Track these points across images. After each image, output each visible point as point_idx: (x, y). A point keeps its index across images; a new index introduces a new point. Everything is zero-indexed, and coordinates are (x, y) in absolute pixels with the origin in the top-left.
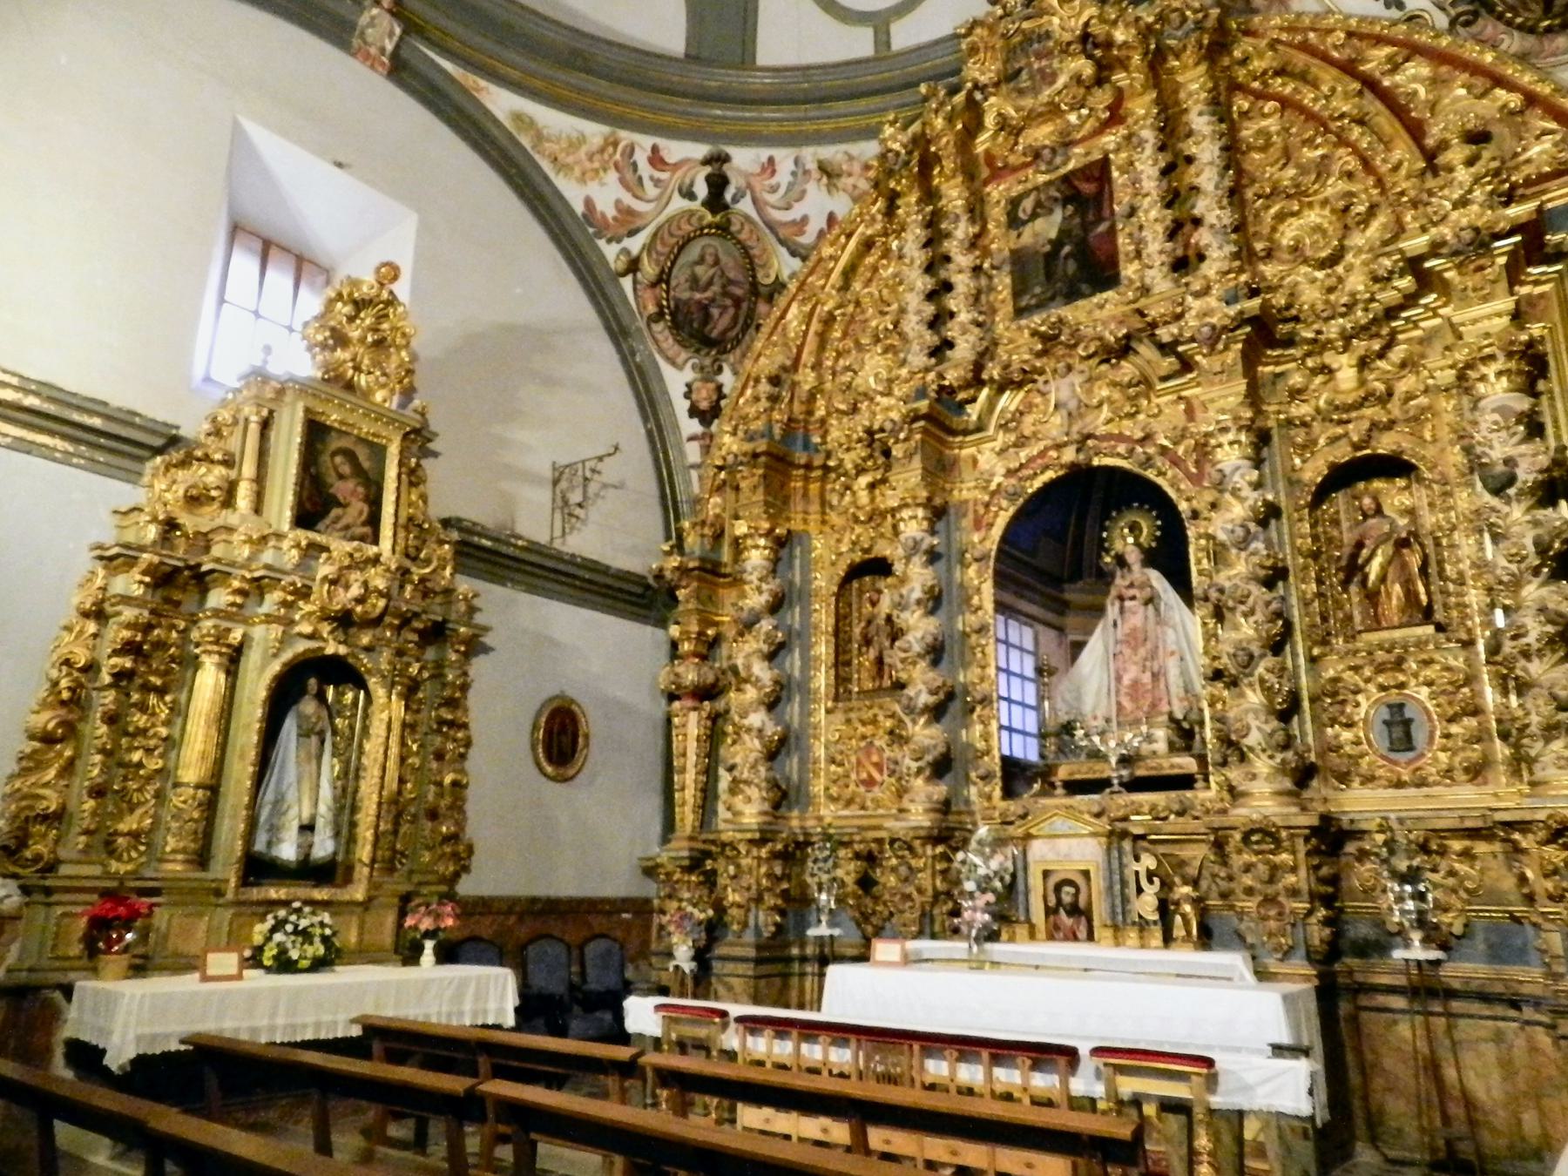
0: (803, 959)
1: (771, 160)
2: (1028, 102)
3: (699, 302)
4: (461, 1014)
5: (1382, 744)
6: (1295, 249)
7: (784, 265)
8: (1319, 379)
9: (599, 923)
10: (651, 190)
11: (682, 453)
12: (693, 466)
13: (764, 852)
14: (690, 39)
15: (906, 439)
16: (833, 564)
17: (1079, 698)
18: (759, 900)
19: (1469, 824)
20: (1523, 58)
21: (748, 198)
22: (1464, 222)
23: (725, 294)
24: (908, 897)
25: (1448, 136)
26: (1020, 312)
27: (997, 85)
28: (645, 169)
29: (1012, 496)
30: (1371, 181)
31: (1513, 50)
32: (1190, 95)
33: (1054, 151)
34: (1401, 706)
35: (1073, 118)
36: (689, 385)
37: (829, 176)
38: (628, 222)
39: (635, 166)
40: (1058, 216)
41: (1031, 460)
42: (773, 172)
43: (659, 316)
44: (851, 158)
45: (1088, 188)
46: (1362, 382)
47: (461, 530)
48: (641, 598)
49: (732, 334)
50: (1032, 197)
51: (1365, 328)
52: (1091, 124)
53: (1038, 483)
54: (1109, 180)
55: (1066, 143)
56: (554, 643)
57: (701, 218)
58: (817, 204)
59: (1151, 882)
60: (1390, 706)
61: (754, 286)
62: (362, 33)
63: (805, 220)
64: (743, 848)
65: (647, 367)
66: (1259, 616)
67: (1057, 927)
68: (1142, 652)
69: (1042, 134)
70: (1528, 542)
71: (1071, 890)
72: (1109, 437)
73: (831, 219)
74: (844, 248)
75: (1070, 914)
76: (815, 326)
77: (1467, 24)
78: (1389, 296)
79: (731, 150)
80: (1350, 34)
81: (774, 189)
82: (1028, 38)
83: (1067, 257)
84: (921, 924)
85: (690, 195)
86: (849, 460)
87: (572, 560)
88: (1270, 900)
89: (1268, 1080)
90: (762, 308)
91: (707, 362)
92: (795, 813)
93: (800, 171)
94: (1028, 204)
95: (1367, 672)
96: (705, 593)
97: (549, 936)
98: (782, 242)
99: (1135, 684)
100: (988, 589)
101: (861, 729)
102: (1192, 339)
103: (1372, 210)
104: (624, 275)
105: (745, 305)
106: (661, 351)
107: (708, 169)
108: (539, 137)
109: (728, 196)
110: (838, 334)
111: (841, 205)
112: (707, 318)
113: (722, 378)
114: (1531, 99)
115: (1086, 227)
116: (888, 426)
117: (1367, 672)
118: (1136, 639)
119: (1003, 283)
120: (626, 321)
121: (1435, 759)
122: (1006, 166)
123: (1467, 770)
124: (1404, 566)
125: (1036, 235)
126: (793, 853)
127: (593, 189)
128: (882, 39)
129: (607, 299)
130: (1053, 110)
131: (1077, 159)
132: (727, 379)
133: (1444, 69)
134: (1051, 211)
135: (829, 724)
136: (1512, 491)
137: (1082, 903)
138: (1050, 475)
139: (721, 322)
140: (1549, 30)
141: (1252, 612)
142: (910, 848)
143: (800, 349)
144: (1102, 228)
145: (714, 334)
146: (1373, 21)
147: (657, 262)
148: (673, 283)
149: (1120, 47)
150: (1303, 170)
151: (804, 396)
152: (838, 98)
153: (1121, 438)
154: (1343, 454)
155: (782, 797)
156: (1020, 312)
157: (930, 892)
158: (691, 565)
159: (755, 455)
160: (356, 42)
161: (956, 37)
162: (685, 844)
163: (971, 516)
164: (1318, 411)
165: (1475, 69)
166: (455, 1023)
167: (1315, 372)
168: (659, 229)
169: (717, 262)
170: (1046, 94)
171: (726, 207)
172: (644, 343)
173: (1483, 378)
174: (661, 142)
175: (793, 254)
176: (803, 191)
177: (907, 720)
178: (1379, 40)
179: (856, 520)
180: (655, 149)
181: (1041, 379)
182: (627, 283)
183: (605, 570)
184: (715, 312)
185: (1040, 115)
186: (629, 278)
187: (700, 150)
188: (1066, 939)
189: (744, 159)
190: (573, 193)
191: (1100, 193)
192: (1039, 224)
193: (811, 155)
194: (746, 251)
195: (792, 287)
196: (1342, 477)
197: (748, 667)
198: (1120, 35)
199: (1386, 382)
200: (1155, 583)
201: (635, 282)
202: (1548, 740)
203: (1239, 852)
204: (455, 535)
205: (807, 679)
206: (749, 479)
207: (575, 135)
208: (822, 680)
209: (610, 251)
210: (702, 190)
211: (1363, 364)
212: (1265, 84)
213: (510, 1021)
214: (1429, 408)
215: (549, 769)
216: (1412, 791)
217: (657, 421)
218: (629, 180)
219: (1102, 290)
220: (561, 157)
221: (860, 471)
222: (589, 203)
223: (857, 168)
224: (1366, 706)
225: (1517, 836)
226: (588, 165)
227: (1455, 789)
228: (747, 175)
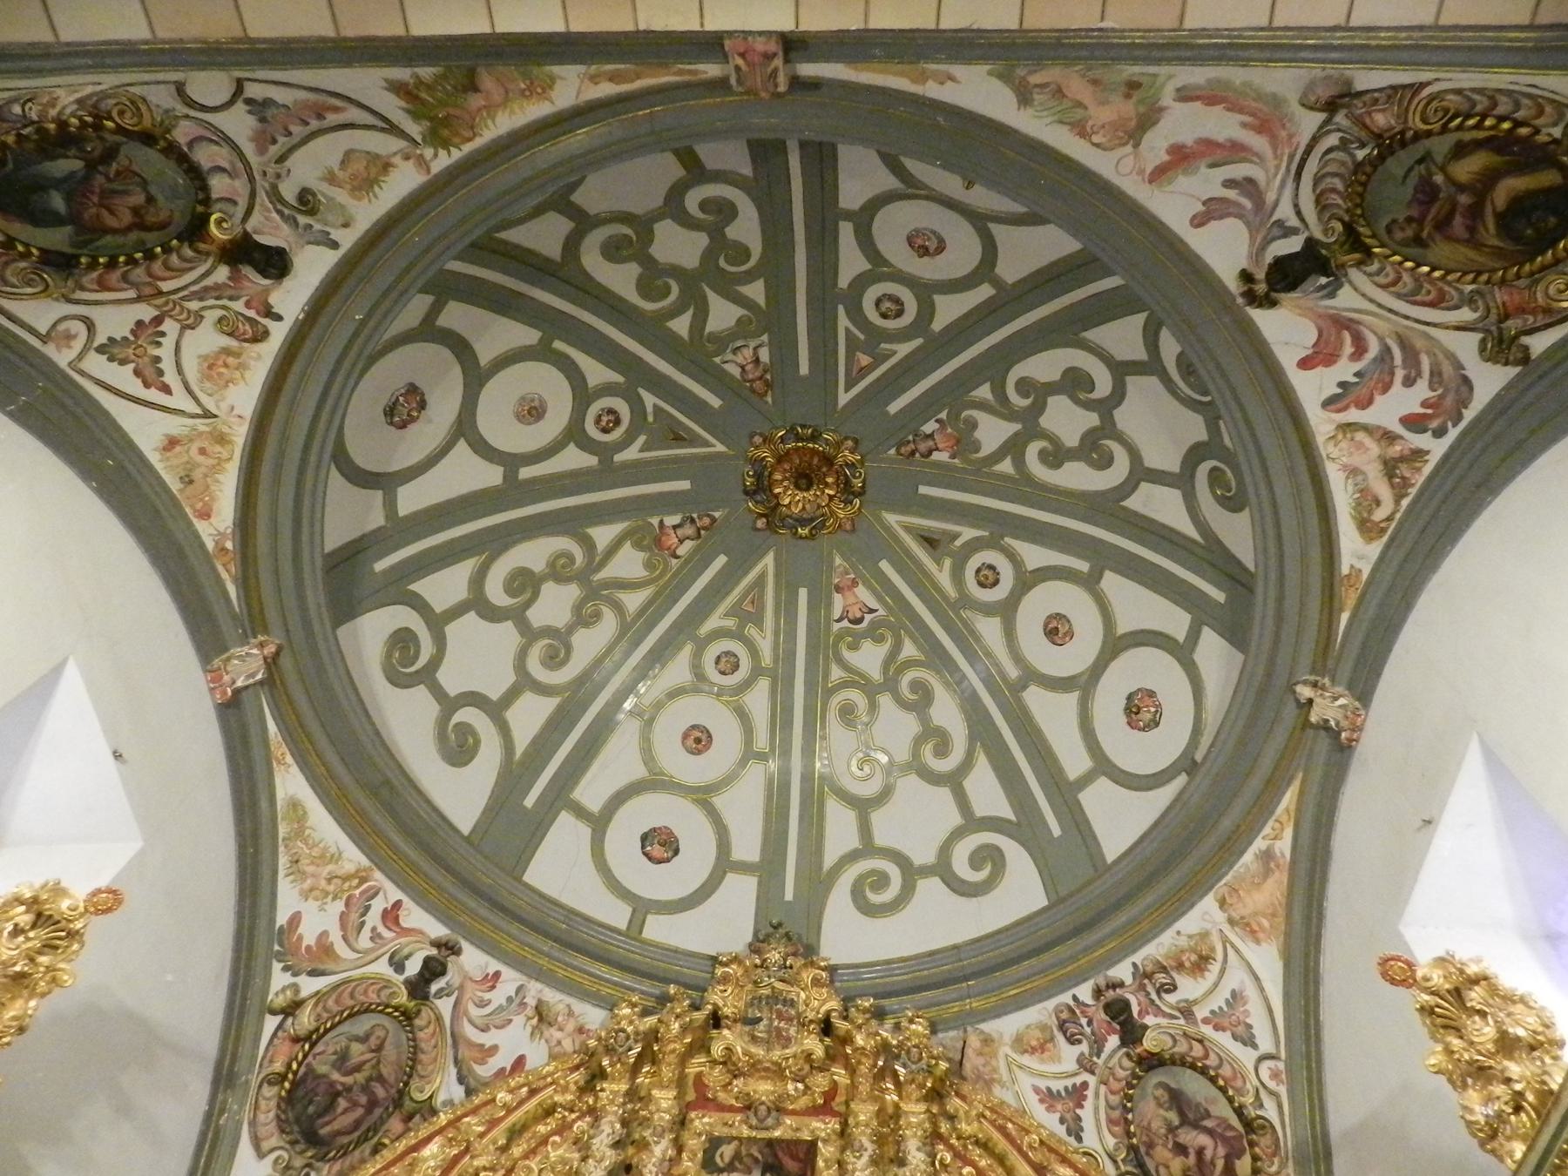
1: (497, 975)
2: (759, 1052)
3: (332, 1084)
7: (446, 1087)
10: (364, 941)
14: (472, 832)
21: (453, 999)
28: (373, 918)
32: (909, 1124)
35: (790, 1087)
37: (541, 1019)
38: (320, 958)
42: (493, 987)
44: (570, 1013)
49: (345, 1140)
50: (735, 1144)
52: (804, 1102)
55: (779, 1109)
58: (514, 1040)
62: (228, 659)
63: (494, 1050)
69: (763, 1089)
73: (520, 1062)
74: (521, 1103)
79: (465, 945)
82: (775, 998)
85: (399, 967)
90: (395, 1124)
91: (298, 1162)
94: (727, 1151)
98: (456, 1062)
104: (274, 1013)
105: (378, 1112)
106: (253, 1123)
107: (434, 952)
108: (299, 833)
109: (434, 988)
111: (537, 1056)
112: (330, 1107)
120: (241, 1065)
127: (309, 909)
128: (637, 923)
129: (239, 1028)
130: (777, 1072)
148: (319, 1048)
149: (855, 1050)
160: (217, 662)
161: (714, 960)
169: (379, 1049)
170: (776, 1054)
171: (426, 997)
172: (242, 1106)
174: (408, 903)
176: (508, 1023)
180: (398, 905)
182: (271, 1023)
184: (342, 1103)
185: (766, 1069)
187: (438, 930)
189: (472, 960)
190: (287, 899)
193: (536, 990)
194: (416, 1049)
195: (443, 1119)
198: (860, 1040)
201: (280, 1026)
207: (333, 850)
209: (279, 979)
210: (413, 967)
218: (345, 916)
220: (304, 861)
222: (295, 919)
223: (570, 1026)
226: (323, 883)
228: (467, 977)
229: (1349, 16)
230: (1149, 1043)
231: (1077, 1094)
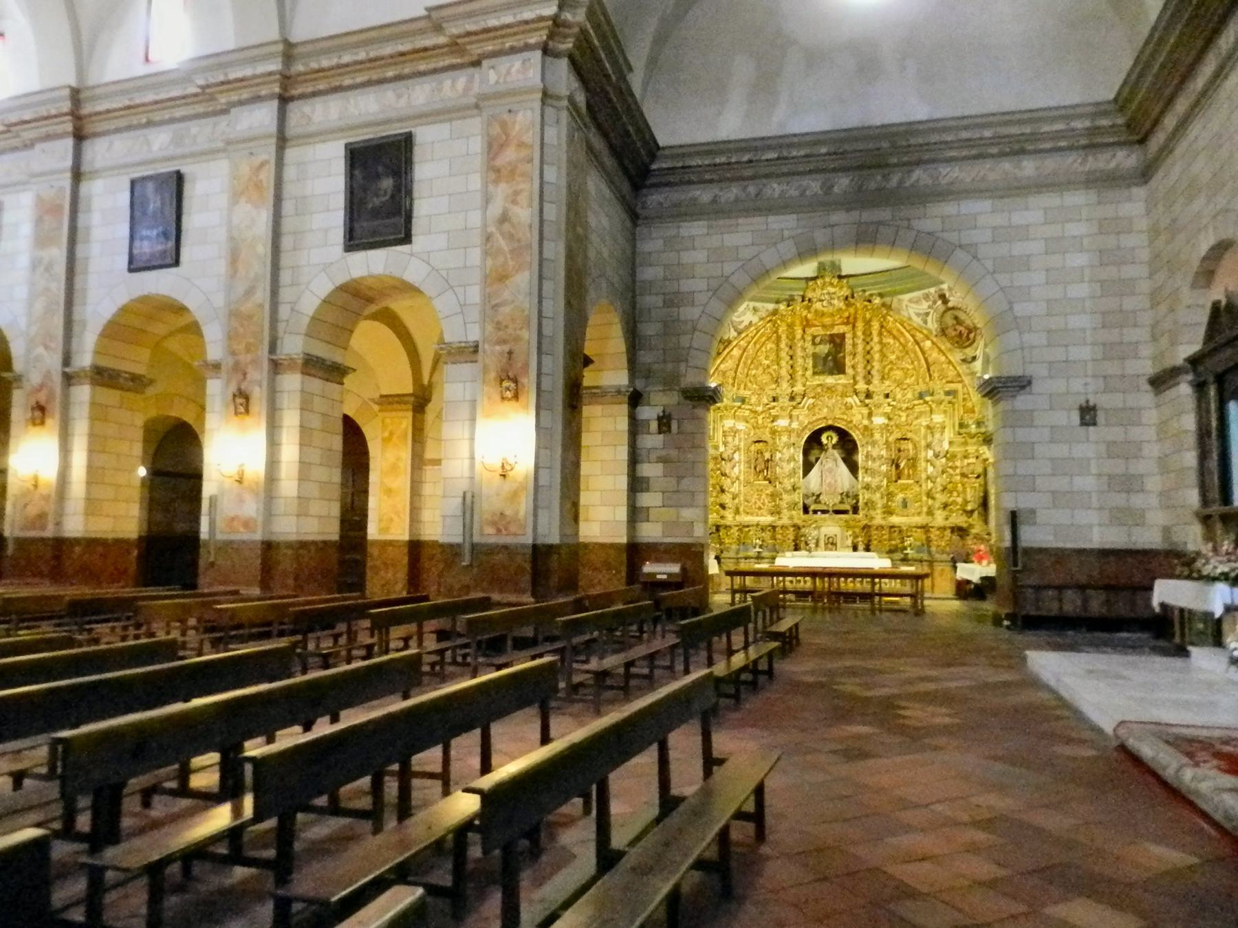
26: (815, 373)
45: (838, 341)
55: (833, 326)
69: (827, 320)
75: (831, 544)
94: (818, 340)
111: (755, 319)
118: (830, 471)
119: (810, 362)
131: (836, 330)
156: (815, 373)
192: (821, 347)
229: (415, 511)
230: (950, 305)
231: (927, 314)
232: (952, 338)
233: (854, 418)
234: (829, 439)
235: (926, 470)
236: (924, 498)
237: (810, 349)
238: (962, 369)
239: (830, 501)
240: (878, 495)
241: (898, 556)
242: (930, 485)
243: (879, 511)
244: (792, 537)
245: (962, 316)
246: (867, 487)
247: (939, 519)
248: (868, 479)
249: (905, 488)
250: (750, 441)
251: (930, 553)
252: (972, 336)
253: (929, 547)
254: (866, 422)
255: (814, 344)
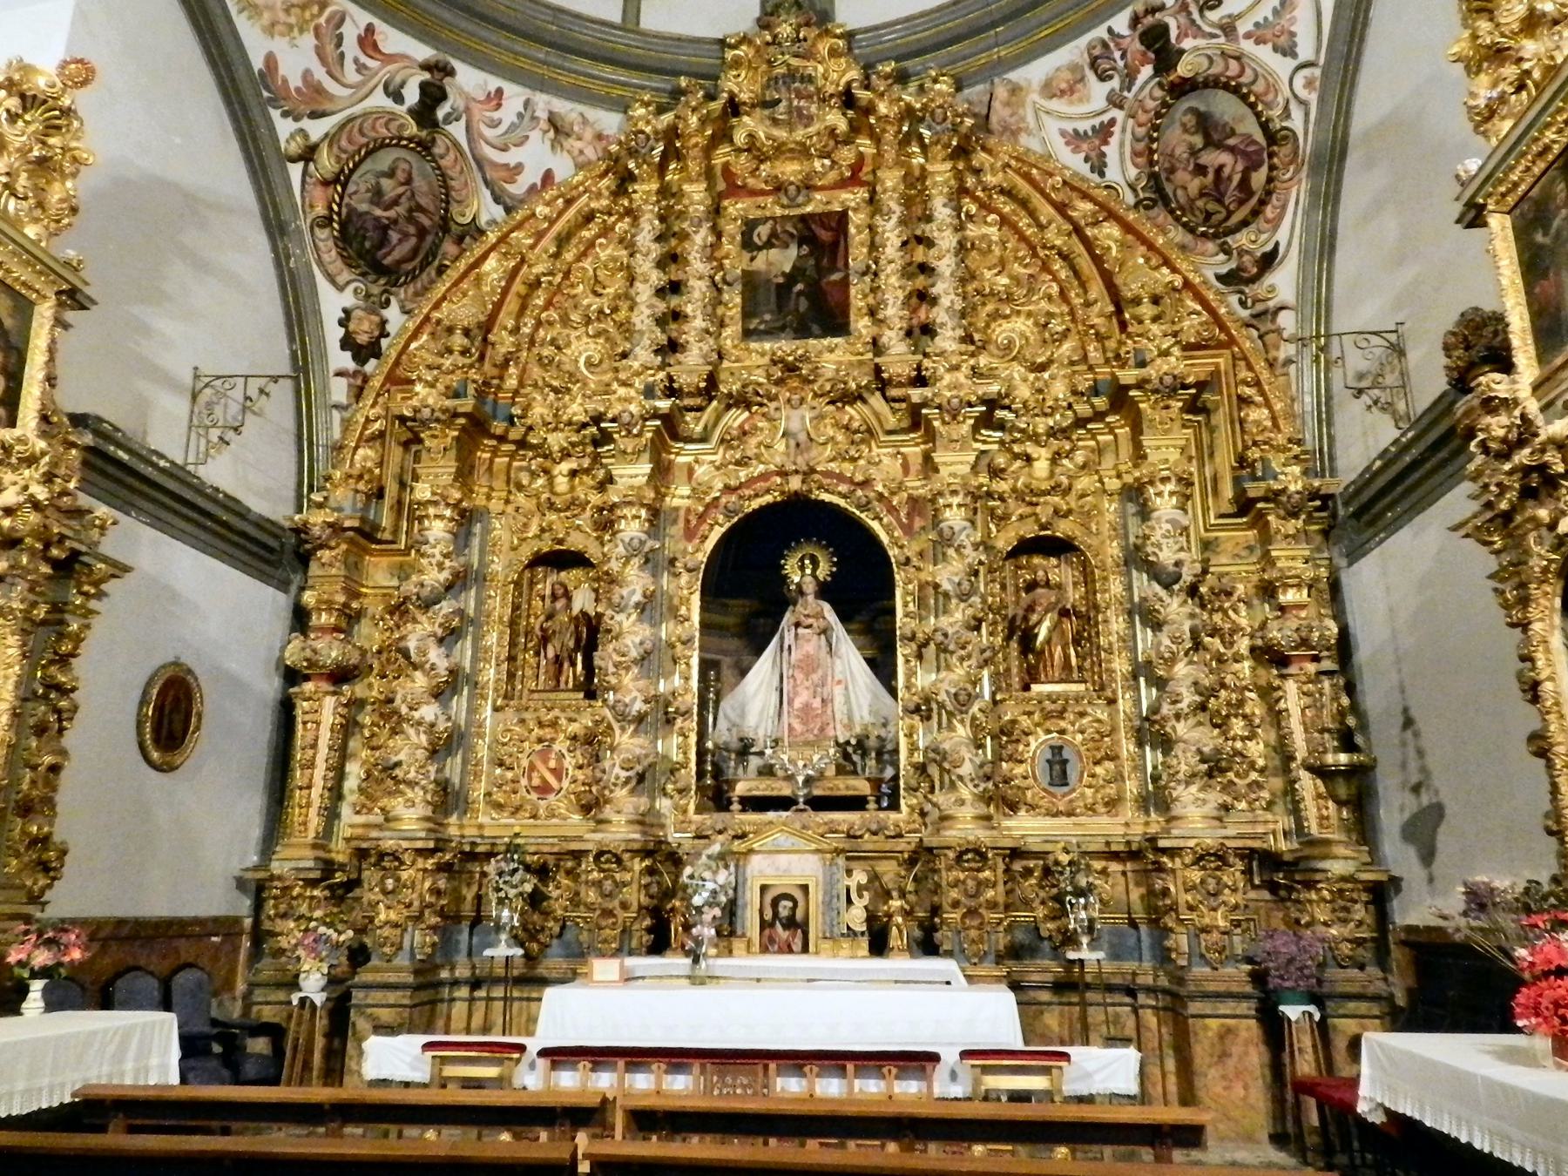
0: (455, 983)
1: (499, 92)
2: (781, 134)
3: (377, 219)
4: (122, 1075)
5: (1044, 780)
6: (1009, 347)
8: (1018, 463)
9: (186, 950)
10: (351, 75)
11: (325, 387)
12: (336, 406)
13: (430, 863)
15: (639, 435)
16: (514, 549)
17: (743, 715)
18: (418, 918)
19: (1114, 848)
20: (1183, 248)
22: (1165, 368)
23: (410, 219)
24: (608, 913)
25: (1143, 294)
26: (748, 334)
27: (753, 106)
28: (351, 48)
29: (729, 513)
30: (1065, 309)
31: (1177, 240)
32: (935, 184)
33: (798, 189)
34: (1061, 748)
35: (817, 164)
36: (347, 312)
37: (557, 130)
38: (314, 102)
39: (340, 38)
40: (793, 252)
41: (751, 481)
42: (499, 106)
43: (326, 221)
45: (825, 235)
46: (1052, 474)
47: (97, 433)
48: (272, 552)
49: (409, 266)
50: (769, 225)
51: (1063, 430)
52: (833, 176)
53: (756, 504)
54: (846, 233)
55: (808, 186)
56: (174, 597)
57: (402, 126)
58: (536, 157)
59: (860, 896)
60: (1052, 747)
61: (445, 224)
63: (519, 168)
64: (407, 858)
65: (302, 273)
66: (973, 662)
67: (772, 940)
68: (815, 677)
69: (790, 170)
70: (1186, 627)
71: (790, 904)
72: (828, 474)
73: (548, 177)
74: (560, 214)
75: (787, 925)
76: (518, 287)
77: (1147, 208)
78: (1083, 409)
79: (457, 65)
80: (1065, 183)
81: (495, 124)
82: (792, 75)
83: (800, 293)
84: (622, 942)
85: (398, 97)
86: (556, 440)
87: (214, 494)
88: (972, 912)
89: (1104, 1067)
90: (449, 247)
91: (375, 290)
92: (453, 819)
93: (527, 112)
94: (763, 231)
95: (1036, 717)
96: (352, 559)
97: (137, 968)
99: (807, 707)
100: (696, 600)
101: (537, 732)
102: (939, 407)
103: (1065, 335)
104: (293, 160)
105: (429, 239)
106: (320, 263)
109: (441, 113)
110: (540, 302)
111: (563, 169)
112: (383, 241)
113: (386, 313)
114: (1187, 284)
115: (821, 271)
116: (626, 418)
117: (1036, 717)
118: (809, 665)
119: (734, 297)
120: (286, 215)
121: (1083, 795)
122: (744, 186)
123: (1106, 804)
124: (1063, 633)
125: (770, 264)
126: (461, 863)
127: (279, 46)
130: (803, 152)
132: (393, 314)
133: (1130, 237)
134: (787, 246)
135: (495, 725)
136: (1176, 587)
137: (799, 915)
138: (768, 499)
139: (398, 250)
140: (1204, 235)
141: (969, 656)
142: (619, 861)
143: (498, 306)
144: (836, 277)
145: (387, 261)
146: (1083, 179)
147: (338, 159)
148: (351, 188)
149: (879, 119)
150: (1016, 280)
151: (499, 359)
152: (585, 55)
153: (841, 478)
154: (1030, 530)
155: (447, 799)
156: (748, 334)
157: (635, 907)
158: (347, 524)
159: (456, 415)
161: (722, 43)
162: (309, 853)
163: (681, 524)
164: (1014, 490)
165: (1151, 246)
166: (115, 1082)
167: (1016, 456)
168: (351, 120)
169: (408, 181)
170: (799, 134)
171: (434, 124)
173: (1159, 494)
174: (376, 22)
175: (497, 200)
177: (616, 726)
178: (1085, 196)
179: (551, 506)
180: (370, 29)
181: (773, 405)
182: (295, 170)
183: (242, 512)
184: (394, 236)
186: (301, 165)
187: (424, 52)
188: (780, 951)
190: (256, 43)
191: (835, 244)
192: (774, 253)
193: (544, 103)
194: (444, 177)
196: (1026, 547)
197: (423, 652)
198: (883, 108)
199: (1069, 477)
200: (827, 615)
201: (305, 173)
202: (1188, 784)
203: (949, 869)
204: (88, 439)
205: (476, 671)
206: (438, 441)
208: (490, 674)
209: (285, 128)
210: (412, 95)
211: (1055, 459)
212: (990, 197)
213: (174, 1079)
214: (1095, 507)
215: (155, 755)
216: (1064, 820)
217: (303, 343)
219: (833, 336)
221: (565, 454)
222: (271, 61)
223: (588, 134)
224: (1037, 745)
225: (1165, 859)
226: (282, 16)
227: (1096, 819)
228: (469, 99)
230: (1183, 69)
231: (1104, 132)
232: (1189, 207)
233: (874, 472)
234: (804, 569)
235: (1129, 642)
236: (1127, 747)
237: (736, 262)
238: (1230, 305)
239: (806, 763)
240: (962, 731)
241: (1042, 969)
242: (1147, 695)
243: (965, 792)
244: (634, 896)
245: (1224, 106)
246: (923, 709)
247: (1195, 816)
248: (925, 679)
249: (1055, 711)
250: (526, 553)
251: (1163, 956)
252: (1259, 178)
253: (1162, 933)
254: (916, 486)
255: (748, 244)
